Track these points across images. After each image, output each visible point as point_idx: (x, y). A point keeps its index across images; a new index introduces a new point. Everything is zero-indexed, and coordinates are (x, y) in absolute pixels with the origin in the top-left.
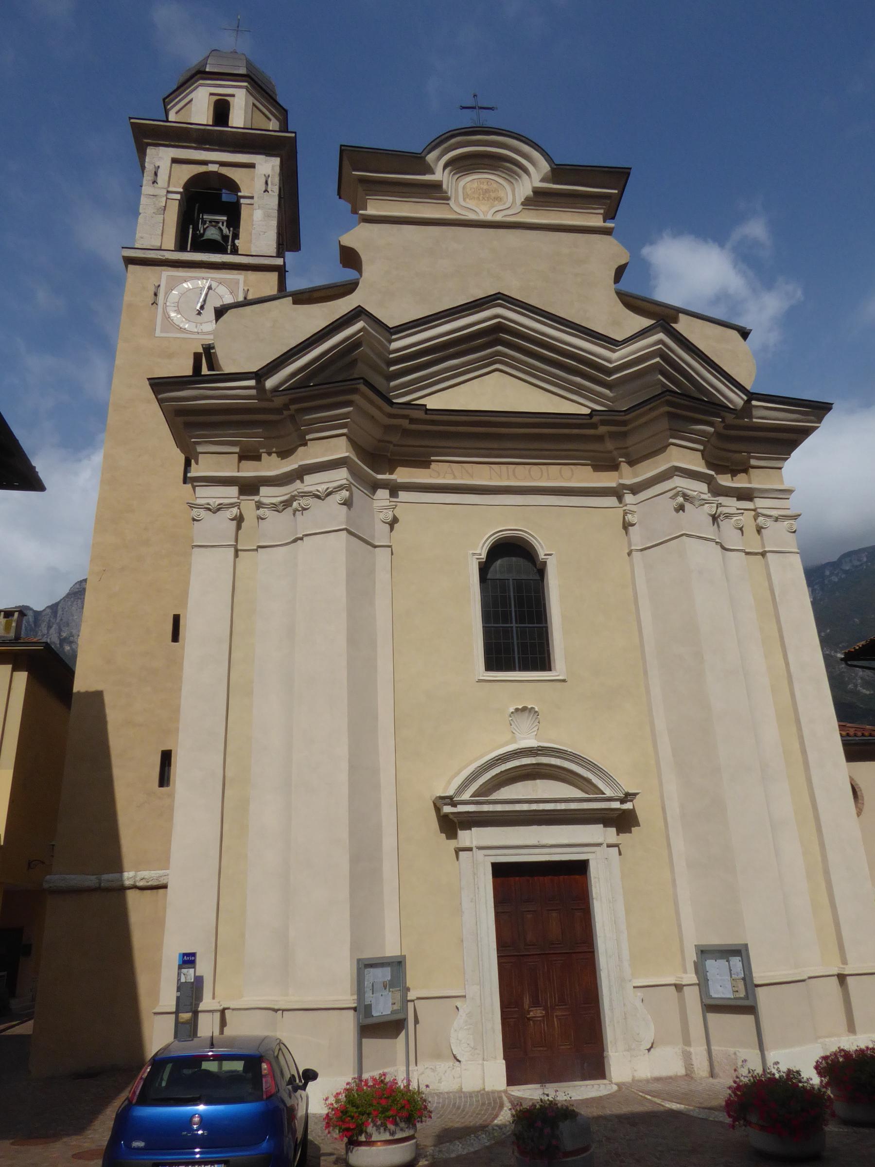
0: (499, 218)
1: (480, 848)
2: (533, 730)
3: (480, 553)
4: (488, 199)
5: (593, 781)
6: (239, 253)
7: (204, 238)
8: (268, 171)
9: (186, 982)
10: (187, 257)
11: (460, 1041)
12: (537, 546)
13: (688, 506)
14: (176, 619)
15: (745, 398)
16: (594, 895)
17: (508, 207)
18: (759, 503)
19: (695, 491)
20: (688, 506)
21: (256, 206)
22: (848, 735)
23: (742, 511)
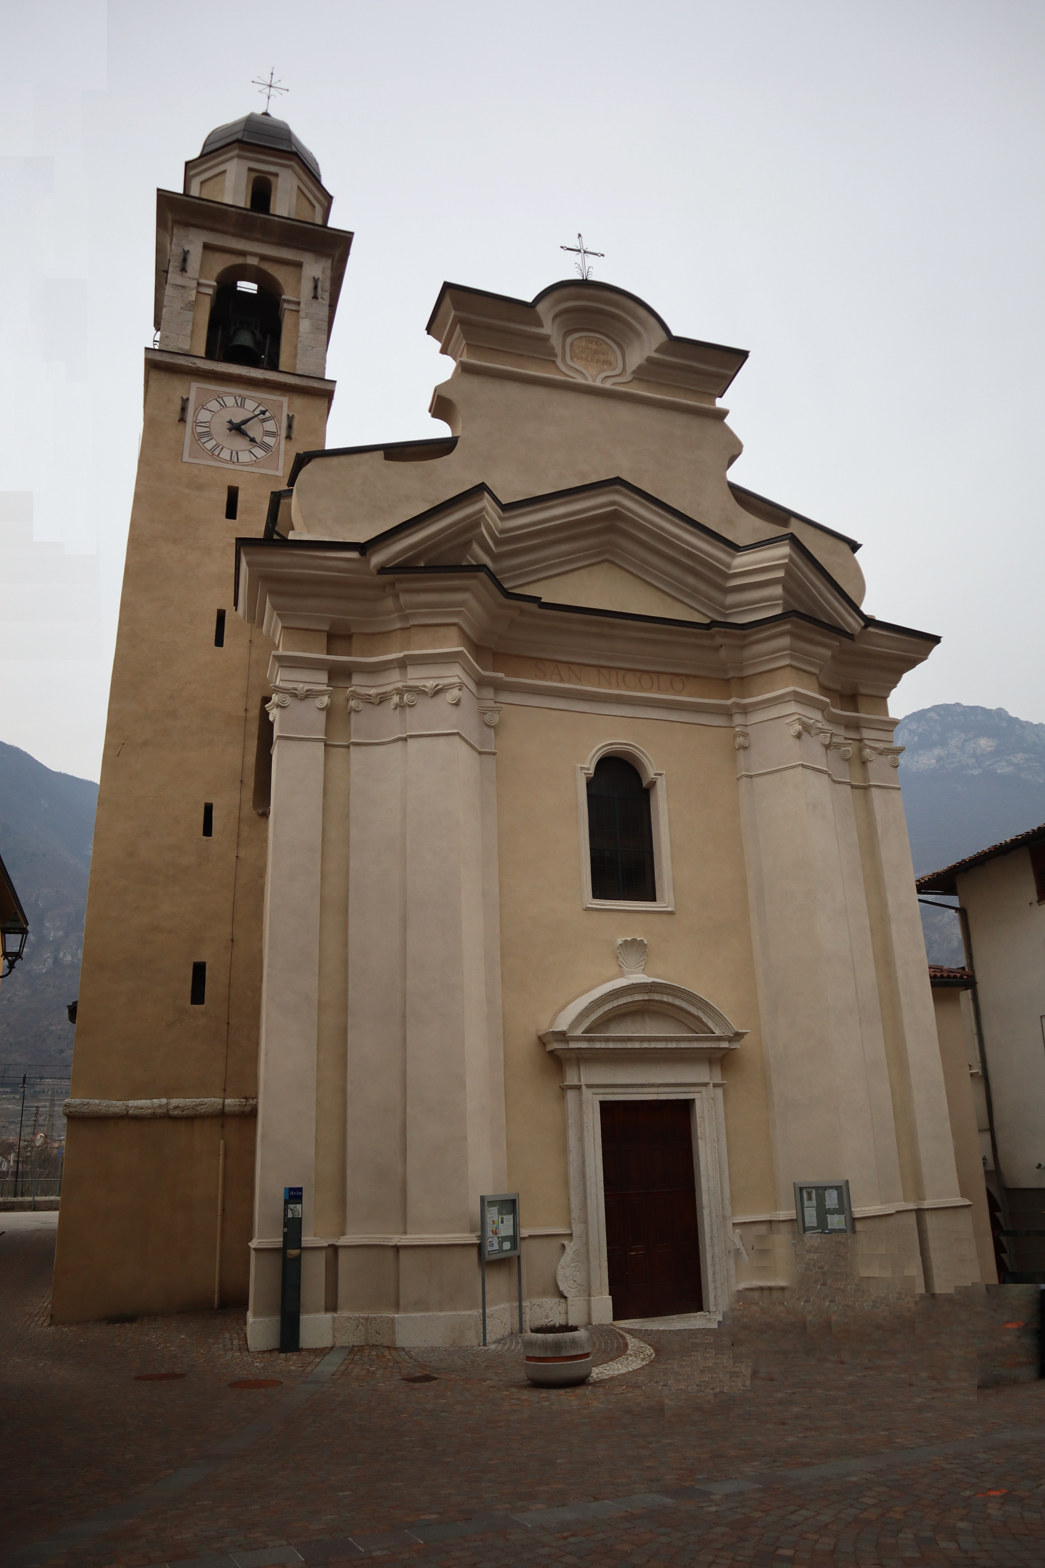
0: (608, 385)
1: (589, 1086)
2: (641, 964)
5: (704, 1019)
6: (281, 369)
7: (233, 344)
8: (318, 274)
10: (224, 368)
13: (805, 735)
15: (863, 624)
16: (699, 1135)
18: (867, 734)
19: (812, 719)
20: (805, 735)
21: (302, 314)
23: (851, 742)
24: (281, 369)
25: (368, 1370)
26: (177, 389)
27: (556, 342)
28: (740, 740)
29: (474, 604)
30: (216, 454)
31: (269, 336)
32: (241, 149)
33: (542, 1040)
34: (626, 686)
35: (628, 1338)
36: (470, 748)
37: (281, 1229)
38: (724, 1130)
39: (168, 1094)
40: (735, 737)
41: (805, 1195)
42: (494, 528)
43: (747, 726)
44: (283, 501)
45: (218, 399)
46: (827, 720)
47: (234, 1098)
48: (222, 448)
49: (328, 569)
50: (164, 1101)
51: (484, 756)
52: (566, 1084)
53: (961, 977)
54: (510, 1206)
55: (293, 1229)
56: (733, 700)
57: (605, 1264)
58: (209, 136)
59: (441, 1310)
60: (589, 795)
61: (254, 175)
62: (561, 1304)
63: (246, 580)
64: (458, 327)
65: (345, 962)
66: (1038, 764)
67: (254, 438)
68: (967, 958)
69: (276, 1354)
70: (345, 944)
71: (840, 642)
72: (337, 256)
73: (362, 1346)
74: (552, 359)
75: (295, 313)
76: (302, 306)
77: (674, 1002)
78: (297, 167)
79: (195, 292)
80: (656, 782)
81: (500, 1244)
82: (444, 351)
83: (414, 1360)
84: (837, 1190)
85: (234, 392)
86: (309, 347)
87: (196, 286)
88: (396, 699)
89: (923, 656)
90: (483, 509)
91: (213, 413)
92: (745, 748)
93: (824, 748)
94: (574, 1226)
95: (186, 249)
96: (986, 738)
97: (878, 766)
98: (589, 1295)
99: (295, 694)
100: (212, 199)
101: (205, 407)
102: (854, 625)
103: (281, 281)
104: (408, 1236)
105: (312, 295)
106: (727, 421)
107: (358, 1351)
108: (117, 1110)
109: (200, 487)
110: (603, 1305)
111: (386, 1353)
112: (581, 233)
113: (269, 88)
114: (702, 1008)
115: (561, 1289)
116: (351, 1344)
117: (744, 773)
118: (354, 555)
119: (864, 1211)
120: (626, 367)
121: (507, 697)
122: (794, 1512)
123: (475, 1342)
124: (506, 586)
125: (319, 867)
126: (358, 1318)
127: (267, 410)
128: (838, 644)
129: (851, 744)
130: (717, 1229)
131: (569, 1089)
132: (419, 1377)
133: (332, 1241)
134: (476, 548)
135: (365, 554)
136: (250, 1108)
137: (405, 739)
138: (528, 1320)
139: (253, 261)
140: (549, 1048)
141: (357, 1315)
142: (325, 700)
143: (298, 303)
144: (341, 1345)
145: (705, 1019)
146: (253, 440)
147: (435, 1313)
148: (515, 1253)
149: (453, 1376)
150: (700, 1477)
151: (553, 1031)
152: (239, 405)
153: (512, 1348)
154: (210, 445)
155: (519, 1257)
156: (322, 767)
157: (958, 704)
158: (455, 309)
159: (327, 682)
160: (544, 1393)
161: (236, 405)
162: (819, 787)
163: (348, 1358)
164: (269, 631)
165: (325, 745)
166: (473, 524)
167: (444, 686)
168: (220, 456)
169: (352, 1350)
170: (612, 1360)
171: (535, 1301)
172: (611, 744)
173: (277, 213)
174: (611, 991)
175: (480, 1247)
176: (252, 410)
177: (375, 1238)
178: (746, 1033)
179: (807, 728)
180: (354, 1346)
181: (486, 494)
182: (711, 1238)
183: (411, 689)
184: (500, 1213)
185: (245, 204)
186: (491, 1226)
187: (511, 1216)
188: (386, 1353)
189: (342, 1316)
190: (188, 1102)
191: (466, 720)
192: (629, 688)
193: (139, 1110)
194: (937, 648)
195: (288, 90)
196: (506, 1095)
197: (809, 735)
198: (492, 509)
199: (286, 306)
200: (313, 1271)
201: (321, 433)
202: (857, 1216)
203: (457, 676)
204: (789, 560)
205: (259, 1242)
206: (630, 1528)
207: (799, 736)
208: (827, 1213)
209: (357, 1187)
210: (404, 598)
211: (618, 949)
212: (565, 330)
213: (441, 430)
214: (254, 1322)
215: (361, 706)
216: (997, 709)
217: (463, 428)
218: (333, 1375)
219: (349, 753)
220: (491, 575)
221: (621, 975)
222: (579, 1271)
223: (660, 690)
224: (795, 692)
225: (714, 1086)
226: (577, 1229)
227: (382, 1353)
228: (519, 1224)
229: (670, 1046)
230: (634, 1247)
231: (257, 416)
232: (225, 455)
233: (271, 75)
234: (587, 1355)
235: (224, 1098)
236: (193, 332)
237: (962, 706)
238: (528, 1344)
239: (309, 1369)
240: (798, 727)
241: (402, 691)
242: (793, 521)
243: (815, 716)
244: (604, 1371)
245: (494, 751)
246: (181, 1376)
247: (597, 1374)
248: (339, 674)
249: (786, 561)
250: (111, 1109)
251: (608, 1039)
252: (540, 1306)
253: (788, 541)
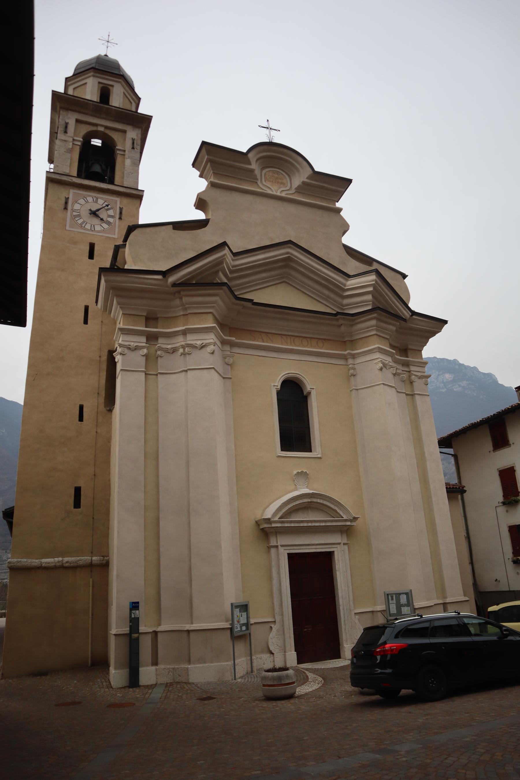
0: (283, 195)
1: (282, 546)
2: (305, 484)
3: (277, 385)
4: (278, 183)
9: (135, 617)
12: (306, 383)
13: (384, 369)
15: (411, 314)
16: (337, 569)
17: (288, 189)
18: (413, 368)
20: (384, 369)
21: (126, 156)
22: (450, 488)
23: (405, 372)
24: (116, 183)
25: (178, 695)
26: (63, 192)
27: (257, 172)
28: (352, 371)
29: (221, 303)
30: (83, 226)
31: (109, 167)
32: (95, 72)
33: (258, 523)
34: (295, 344)
35: (307, 673)
36: (219, 376)
37: (128, 624)
38: (349, 566)
39: (63, 555)
40: (349, 370)
41: (390, 598)
42: (229, 265)
43: (355, 364)
44: (121, 250)
45: (84, 198)
46: (394, 362)
47: (97, 557)
48: (86, 223)
49: (146, 284)
50: (60, 559)
52: (270, 545)
53: (459, 488)
54: (244, 608)
55: (134, 623)
56: (348, 351)
57: (292, 636)
58: (78, 65)
59: (212, 663)
60: (278, 400)
61: (101, 85)
62: (271, 657)
63: (103, 290)
64: (209, 164)
65: (158, 485)
66: (473, 386)
67: (103, 218)
68: (458, 479)
69: (127, 689)
70: (157, 476)
71: (400, 323)
72: (144, 128)
73: (171, 683)
74: (256, 181)
75: (123, 156)
76: (127, 152)
77: (323, 503)
78: (123, 83)
79: (71, 144)
80: (311, 392)
81: (241, 627)
82: (201, 176)
83: (200, 689)
84: (406, 594)
85: (92, 195)
86: (130, 173)
87: (72, 140)
88: (181, 350)
89: (439, 330)
90: (225, 255)
91: (81, 205)
92: (354, 375)
93: (393, 375)
94: (276, 617)
95: (67, 121)
96: (449, 374)
97: (418, 384)
98: (285, 652)
99: (130, 348)
100: (79, 96)
101: (77, 202)
102: (407, 314)
103: (116, 140)
104: (194, 625)
105: (131, 147)
106: (342, 213)
107: (170, 686)
108: (36, 564)
109: (75, 243)
110: (292, 657)
111: (185, 686)
112: (268, 119)
113: (107, 42)
114: (337, 506)
115: (271, 649)
116: (165, 682)
117: (354, 388)
118: (160, 277)
120: (292, 185)
122: (446, 759)
123: (230, 678)
124: (236, 293)
125: (143, 437)
126: (169, 669)
127: (109, 204)
128: (399, 324)
129: (405, 373)
130: (347, 616)
131: (272, 547)
132: (205, 698)
133: (154, 629)
134: (221, 274)
135: (165, 277)
136: (106, 562)
137: (186, 371)
138: (255, 666)
139: (101, 129)
140: (261, 527)
141: (168, 667)
142: (145, 351)
143: (124, 151)
144: (161, 683)
145: (338, 511)
146: (102, 219)
147: (209, 664)
148: (248, 632)
149: (223, 696)
150: (387, 743)
151: (264, 519)
152: (95, 201)
153: (250, 681)
154: (80, 221)
155: (250, 634)
156: (144, 385)
157: (435, 358)
158: (207, 155)
159: (145, 341)
160: (274, 703)
161: (93, 202)
162: (391, 395)
163: (166, 689)
164: (114, 316)
165: (146, 374)
166: (220, 262)
167: (206, 344)
168: (85, 227)
169: (167, 685)
170: (302, 684)
171: (258, 656)
173: (113, 105)
174: (292, 498)
175: (231, 629)
176: (101, 204)
177: (176, 627)
178: (359, 517)
179: (385, 365)
180: (167, 683)
181: (227, 247)
182: (344, 621)
183: (189, 345)
184: (240, 612)
185: (97, 100)
186: (236, 618)
187: (245, 613)
188: (185, 686)
189: (160, 668)
190: (73, 559)
191: (216, 361)
192: (296, 346)
193: (47, 564)
194: (446, 326)
195: (117, 44)
196: (241, 552)
198: (229, 255)
199: (118, 152)
200: (145, 644)
201: (136, 215)
202: (416, 607)
203: (213, 339)
204: (375, 282)
205: (117, 631)
206: (366, 772)
207: (381, 369)
208: (401, 606)
209: (166, 600)
210: (185, 299)
211: (294, 476)
212: (261, 167)
213: (200, 215)
214: (115, 673)
215: (163, 354)
216: (454, 360)
217: (212, 215)
218: (160, 699)
219: (157, 378)
220: (229, 288)
221: (296, 489)
222: (279, 640)
223: (311, 347)
224: (379, 347)
225: (343, 545)
226: (278, 618)
227: (183, 686)
228: (249, 617)
229: (322, 525)
230: (306, 626)
231: (104, 207)
232: (88, 227)
233: (108, 36)
234: (293, 683)
235: (92, 557)
236: (71, 164)
237: (437, 358)
238: (264, 678)
239: (147, 696)
240: (381, 365)
241: (184, 346)
242: (374, 263)
243: (388, 359)
244: (301, 690)
245: (230, 377)
246: (79, 703)
247: (298, 692)
248: (152, 338)
249: (374, 282)
250: (33, 564)
251: (291, 522)
252: (261, 658)
253: (374, 273)
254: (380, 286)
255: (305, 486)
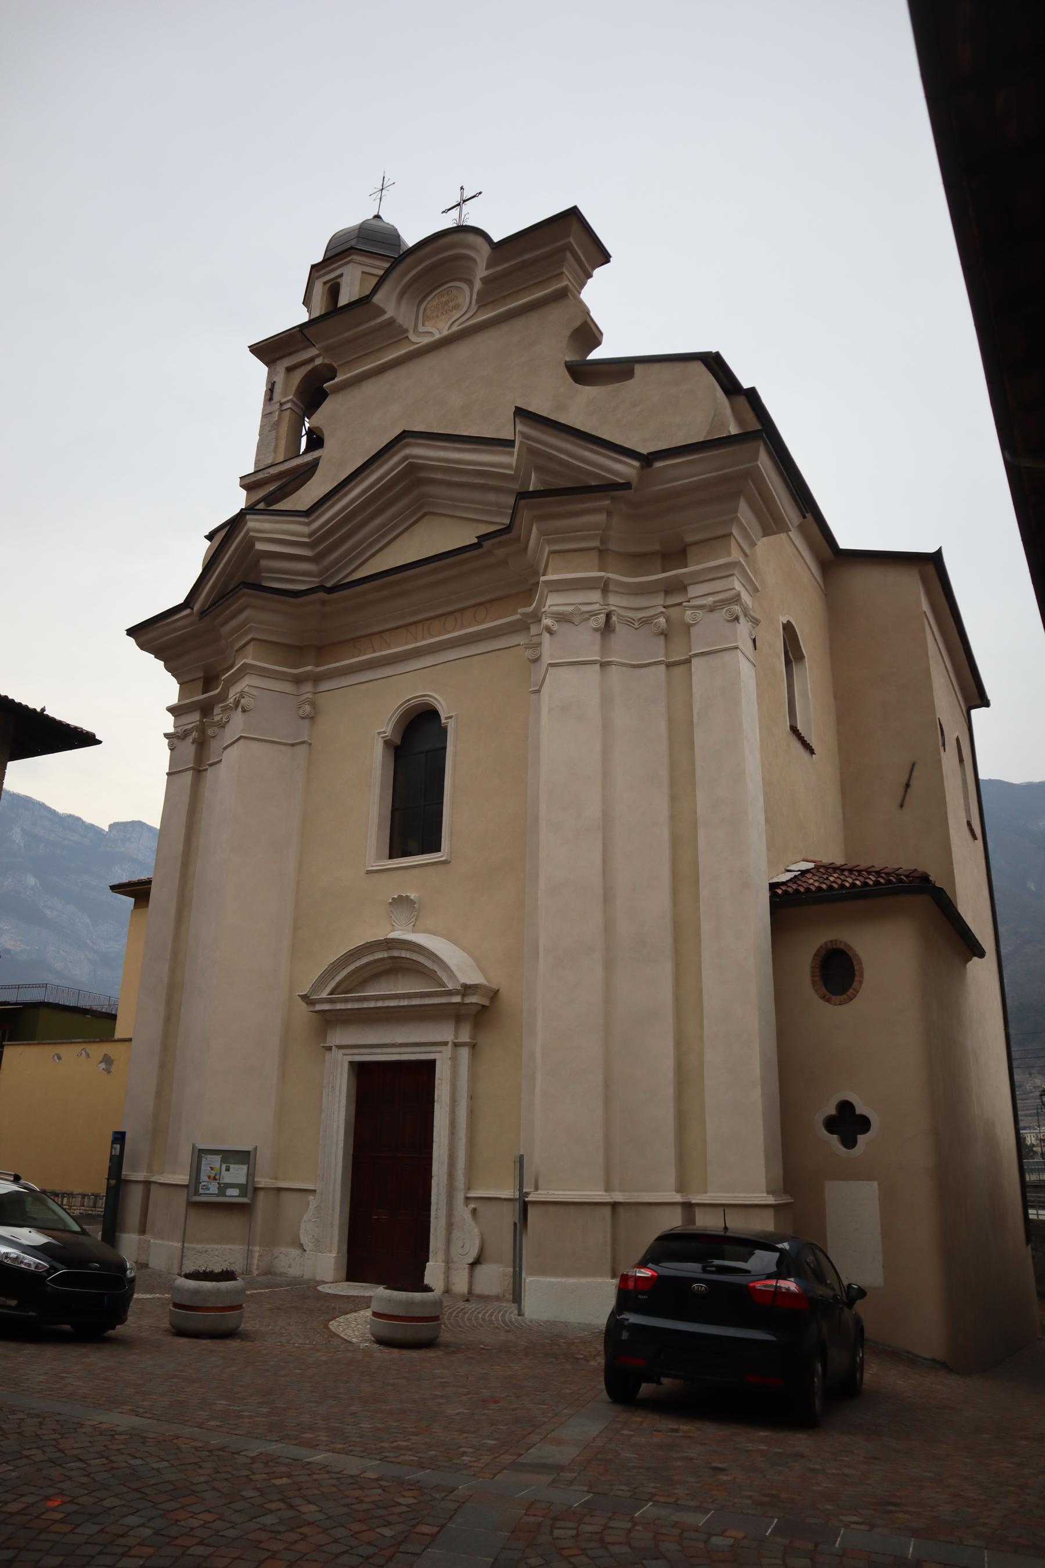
0: (455, 328)
1: (339, 1047)
2: (412, 920)
11: (308, 1232)
14: (755, 649)
15: (636, 464)
51: (295, 748)
61: (328, 285)
102: (625, 469)
119: (553, 1194)
121: (324, 686)
172: (409, 700)
197: (571, 624)
200: (134, 1197)
229: (402, 1004)
254: (536, 440)
255: (410, 925)
